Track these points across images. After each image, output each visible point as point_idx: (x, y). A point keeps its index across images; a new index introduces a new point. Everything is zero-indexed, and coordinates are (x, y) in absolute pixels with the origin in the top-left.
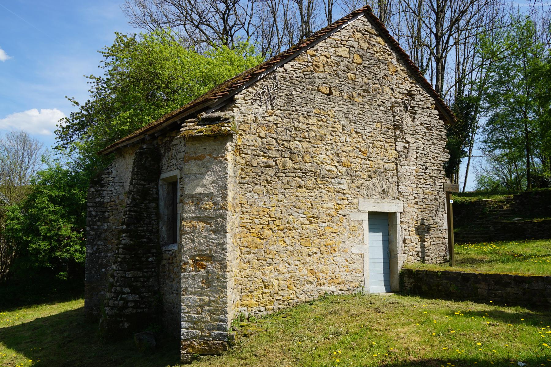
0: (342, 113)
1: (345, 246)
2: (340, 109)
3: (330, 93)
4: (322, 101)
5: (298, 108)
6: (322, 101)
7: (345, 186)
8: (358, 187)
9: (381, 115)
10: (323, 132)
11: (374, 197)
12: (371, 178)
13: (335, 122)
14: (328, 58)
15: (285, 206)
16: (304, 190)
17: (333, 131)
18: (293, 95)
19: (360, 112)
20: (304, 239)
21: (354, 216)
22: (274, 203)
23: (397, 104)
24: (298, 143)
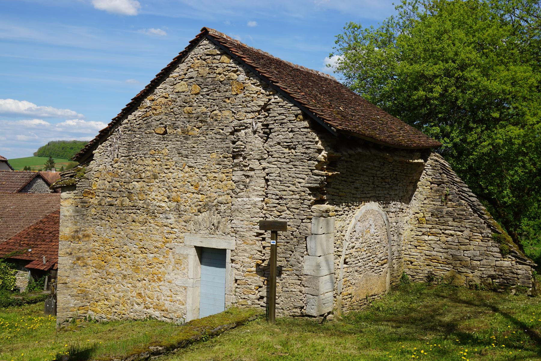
0: (174, 150)
1: (169, 277)
2: (173, 146)
3: (165, 133)
4: (157, 141)
5: (137, 153)
6: (157, 141)
7: (172, 221)
8: (185, 222)
9: (217, 144)
10: (157, 171)
11: (202, 232)
12: (201, 213)
13: (168, 160)
14: (166, 98)
15: (122, 238)
16: (138, 224)
17: (166, 169)
18: (133, 142)
19: (193, 145)
20: (136, 267)
21: (179, 249)
22: (114, 234)
23: (242, 126)
24: (136, 183)
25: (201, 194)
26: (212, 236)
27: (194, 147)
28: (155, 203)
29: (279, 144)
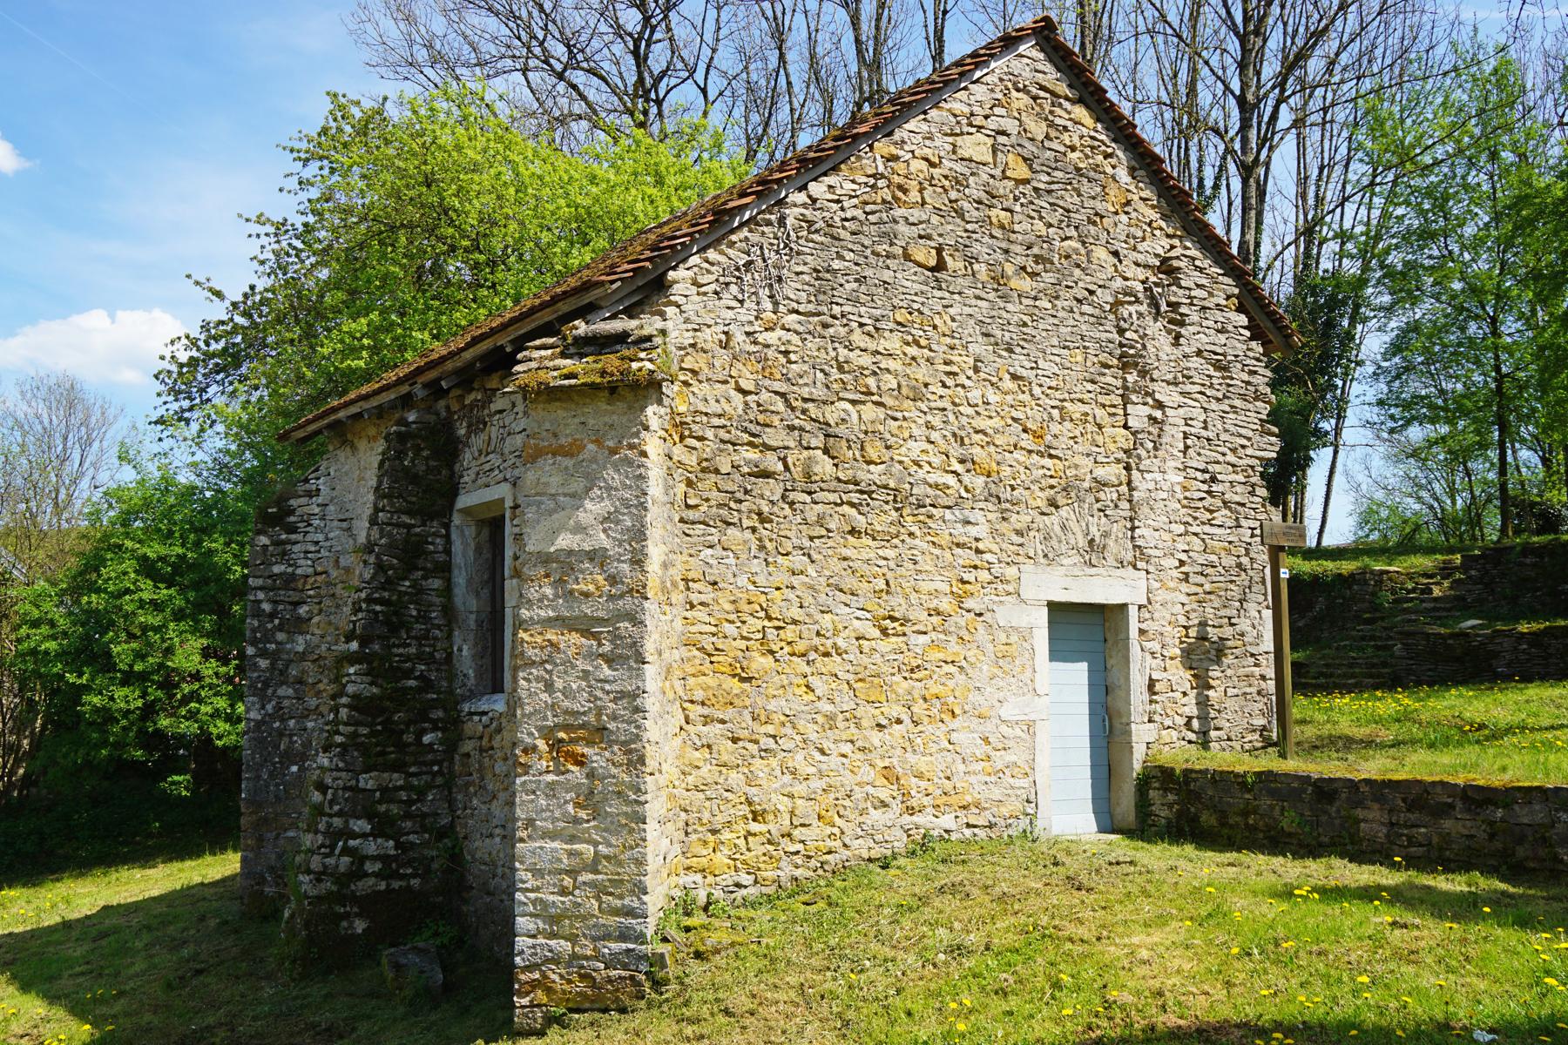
2: (967, 310)
3: (940, 266)
4: (917, 287)
5: (847, 309)
6: (917, 287)
7: (981, 530)
8: (1019, 533)
9: (1084, 327)
12: (1057, 507)
14: (932, 165)
17: (948, 374)
19: (1026, 318)
21: (1007, 614)
22: (782, 578)
25: (1051, 456)
26: (1093, 571)
27: (1025, 325)
28: (921, 474)
29: (1199, 353)
